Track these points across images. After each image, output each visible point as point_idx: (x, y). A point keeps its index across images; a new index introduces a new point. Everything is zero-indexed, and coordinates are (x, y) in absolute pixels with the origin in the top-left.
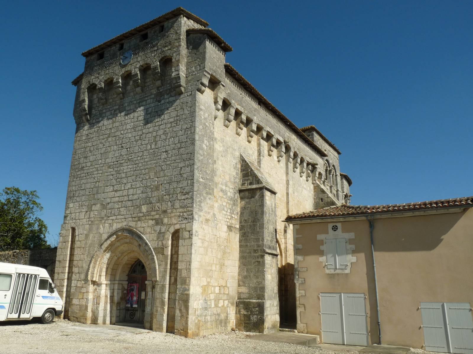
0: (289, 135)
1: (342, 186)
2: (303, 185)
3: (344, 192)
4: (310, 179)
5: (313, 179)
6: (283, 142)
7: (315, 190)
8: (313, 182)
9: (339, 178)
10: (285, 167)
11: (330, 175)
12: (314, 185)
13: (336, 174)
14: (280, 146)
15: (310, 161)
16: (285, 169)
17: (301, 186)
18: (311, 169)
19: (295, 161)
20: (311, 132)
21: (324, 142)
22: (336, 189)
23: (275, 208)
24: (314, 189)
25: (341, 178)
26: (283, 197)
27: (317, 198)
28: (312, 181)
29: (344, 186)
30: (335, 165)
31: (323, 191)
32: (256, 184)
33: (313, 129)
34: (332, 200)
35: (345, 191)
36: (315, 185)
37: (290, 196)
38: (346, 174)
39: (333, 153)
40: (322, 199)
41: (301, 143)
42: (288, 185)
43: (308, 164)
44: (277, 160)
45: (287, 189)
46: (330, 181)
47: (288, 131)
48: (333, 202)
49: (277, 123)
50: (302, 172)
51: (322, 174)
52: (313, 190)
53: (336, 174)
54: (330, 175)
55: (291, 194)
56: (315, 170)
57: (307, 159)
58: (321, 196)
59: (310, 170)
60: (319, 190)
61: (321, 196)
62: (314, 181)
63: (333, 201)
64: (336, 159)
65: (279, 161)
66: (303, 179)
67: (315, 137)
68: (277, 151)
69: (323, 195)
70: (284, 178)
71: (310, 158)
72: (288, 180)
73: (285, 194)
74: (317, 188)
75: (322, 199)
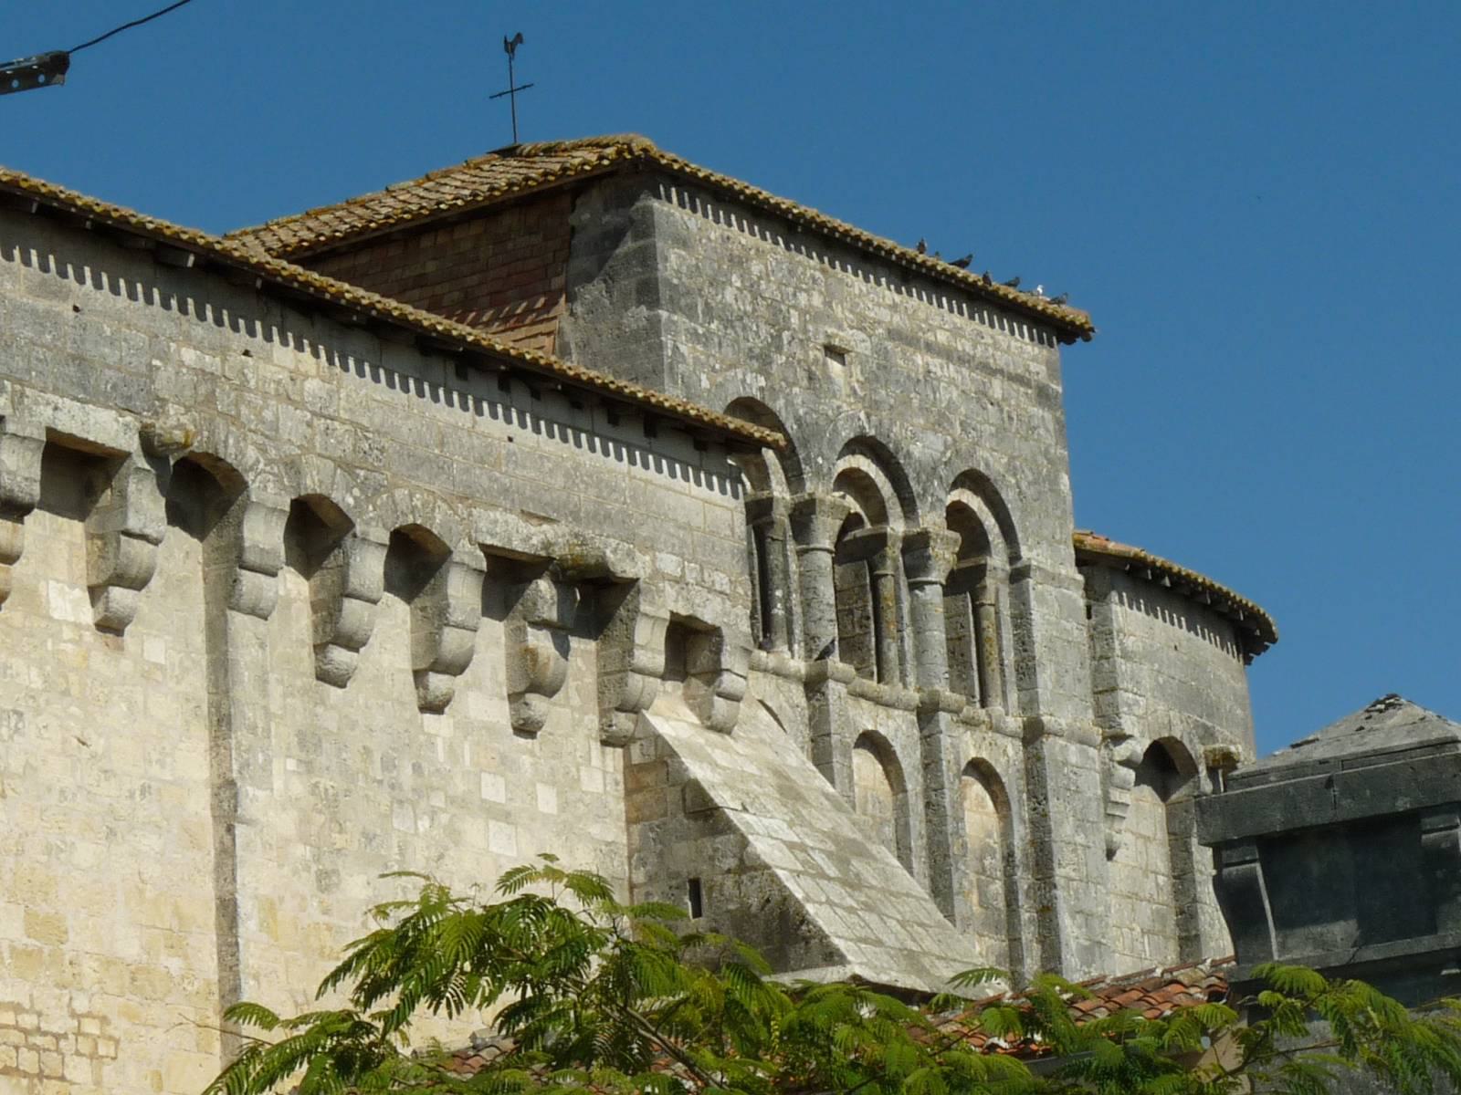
0: (211, 362)
1: (1096, 671)
2: (460, 786)
3: (1119, 738)
4: (572, 714)
5: (613, 699)
6: (131, 444)
7: (638, 798)
8: (606, 726)
9: (1056, 601)
10: (203, 660)
11: (914, 586)
12: (627, 757)
13: (1014, 557)
14: (108, 483)
15: (524, 537)
16: (197, 682)
17: (438, 800)
18: (552, 614)
19: (325, 576)
20: (634, 198)
21: (810, 265)
22: (1014, 722)
23: (799, 815)
24: (629, 793)
25: (1089, 589)
26: (175, 944)
27: (651, 879)
28: (603, 713)
29: (1123, 666)
30: (990, 461)
31: (703, 813)
32: (769, 487)
33: (637, 175)
34: (776, 897)
35: (1128, 724)
36: (636, 758)
37: (249, 927)
38: (1134, 550)
39: (964, 346)
40: (695, 887)
41: (380, 391)
42: (230, 829)
43: (507, 576)
44: (88, 615)
45: (219, 866)
46: (920, 653)
47: (191, 324)
48: (784, 916)
49: (43, 290)
50: (436, 664)
51: (713, 633)
52: (619, 807)
53: (1014, 557)
54: (914, 586)
55: (270, 908)
56: (622, 612)
57: (476, 528)
58: (686, 855)
59: (541, 624)
60: (673, 795)
61: (686, 855)
62: (623, 722)
63: (787, 898)
64: (1022, 400)
65: (111, 626)
66: (465, 727)
67: (683, 243)
68: (90, 536)
69: (708, 844)
70: (193, 763)
71: (528, 516)
72: (232, 783)
73: (208, 915)
74: (648, 779)
75: (695, 887)
